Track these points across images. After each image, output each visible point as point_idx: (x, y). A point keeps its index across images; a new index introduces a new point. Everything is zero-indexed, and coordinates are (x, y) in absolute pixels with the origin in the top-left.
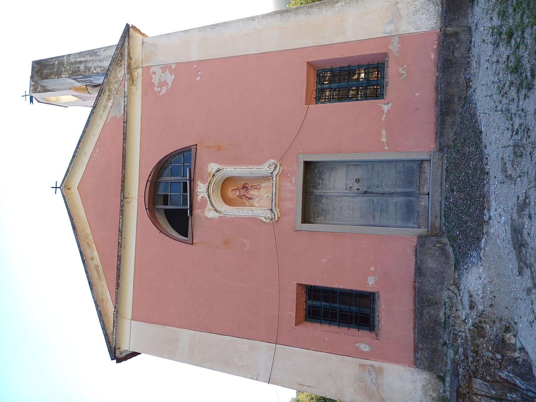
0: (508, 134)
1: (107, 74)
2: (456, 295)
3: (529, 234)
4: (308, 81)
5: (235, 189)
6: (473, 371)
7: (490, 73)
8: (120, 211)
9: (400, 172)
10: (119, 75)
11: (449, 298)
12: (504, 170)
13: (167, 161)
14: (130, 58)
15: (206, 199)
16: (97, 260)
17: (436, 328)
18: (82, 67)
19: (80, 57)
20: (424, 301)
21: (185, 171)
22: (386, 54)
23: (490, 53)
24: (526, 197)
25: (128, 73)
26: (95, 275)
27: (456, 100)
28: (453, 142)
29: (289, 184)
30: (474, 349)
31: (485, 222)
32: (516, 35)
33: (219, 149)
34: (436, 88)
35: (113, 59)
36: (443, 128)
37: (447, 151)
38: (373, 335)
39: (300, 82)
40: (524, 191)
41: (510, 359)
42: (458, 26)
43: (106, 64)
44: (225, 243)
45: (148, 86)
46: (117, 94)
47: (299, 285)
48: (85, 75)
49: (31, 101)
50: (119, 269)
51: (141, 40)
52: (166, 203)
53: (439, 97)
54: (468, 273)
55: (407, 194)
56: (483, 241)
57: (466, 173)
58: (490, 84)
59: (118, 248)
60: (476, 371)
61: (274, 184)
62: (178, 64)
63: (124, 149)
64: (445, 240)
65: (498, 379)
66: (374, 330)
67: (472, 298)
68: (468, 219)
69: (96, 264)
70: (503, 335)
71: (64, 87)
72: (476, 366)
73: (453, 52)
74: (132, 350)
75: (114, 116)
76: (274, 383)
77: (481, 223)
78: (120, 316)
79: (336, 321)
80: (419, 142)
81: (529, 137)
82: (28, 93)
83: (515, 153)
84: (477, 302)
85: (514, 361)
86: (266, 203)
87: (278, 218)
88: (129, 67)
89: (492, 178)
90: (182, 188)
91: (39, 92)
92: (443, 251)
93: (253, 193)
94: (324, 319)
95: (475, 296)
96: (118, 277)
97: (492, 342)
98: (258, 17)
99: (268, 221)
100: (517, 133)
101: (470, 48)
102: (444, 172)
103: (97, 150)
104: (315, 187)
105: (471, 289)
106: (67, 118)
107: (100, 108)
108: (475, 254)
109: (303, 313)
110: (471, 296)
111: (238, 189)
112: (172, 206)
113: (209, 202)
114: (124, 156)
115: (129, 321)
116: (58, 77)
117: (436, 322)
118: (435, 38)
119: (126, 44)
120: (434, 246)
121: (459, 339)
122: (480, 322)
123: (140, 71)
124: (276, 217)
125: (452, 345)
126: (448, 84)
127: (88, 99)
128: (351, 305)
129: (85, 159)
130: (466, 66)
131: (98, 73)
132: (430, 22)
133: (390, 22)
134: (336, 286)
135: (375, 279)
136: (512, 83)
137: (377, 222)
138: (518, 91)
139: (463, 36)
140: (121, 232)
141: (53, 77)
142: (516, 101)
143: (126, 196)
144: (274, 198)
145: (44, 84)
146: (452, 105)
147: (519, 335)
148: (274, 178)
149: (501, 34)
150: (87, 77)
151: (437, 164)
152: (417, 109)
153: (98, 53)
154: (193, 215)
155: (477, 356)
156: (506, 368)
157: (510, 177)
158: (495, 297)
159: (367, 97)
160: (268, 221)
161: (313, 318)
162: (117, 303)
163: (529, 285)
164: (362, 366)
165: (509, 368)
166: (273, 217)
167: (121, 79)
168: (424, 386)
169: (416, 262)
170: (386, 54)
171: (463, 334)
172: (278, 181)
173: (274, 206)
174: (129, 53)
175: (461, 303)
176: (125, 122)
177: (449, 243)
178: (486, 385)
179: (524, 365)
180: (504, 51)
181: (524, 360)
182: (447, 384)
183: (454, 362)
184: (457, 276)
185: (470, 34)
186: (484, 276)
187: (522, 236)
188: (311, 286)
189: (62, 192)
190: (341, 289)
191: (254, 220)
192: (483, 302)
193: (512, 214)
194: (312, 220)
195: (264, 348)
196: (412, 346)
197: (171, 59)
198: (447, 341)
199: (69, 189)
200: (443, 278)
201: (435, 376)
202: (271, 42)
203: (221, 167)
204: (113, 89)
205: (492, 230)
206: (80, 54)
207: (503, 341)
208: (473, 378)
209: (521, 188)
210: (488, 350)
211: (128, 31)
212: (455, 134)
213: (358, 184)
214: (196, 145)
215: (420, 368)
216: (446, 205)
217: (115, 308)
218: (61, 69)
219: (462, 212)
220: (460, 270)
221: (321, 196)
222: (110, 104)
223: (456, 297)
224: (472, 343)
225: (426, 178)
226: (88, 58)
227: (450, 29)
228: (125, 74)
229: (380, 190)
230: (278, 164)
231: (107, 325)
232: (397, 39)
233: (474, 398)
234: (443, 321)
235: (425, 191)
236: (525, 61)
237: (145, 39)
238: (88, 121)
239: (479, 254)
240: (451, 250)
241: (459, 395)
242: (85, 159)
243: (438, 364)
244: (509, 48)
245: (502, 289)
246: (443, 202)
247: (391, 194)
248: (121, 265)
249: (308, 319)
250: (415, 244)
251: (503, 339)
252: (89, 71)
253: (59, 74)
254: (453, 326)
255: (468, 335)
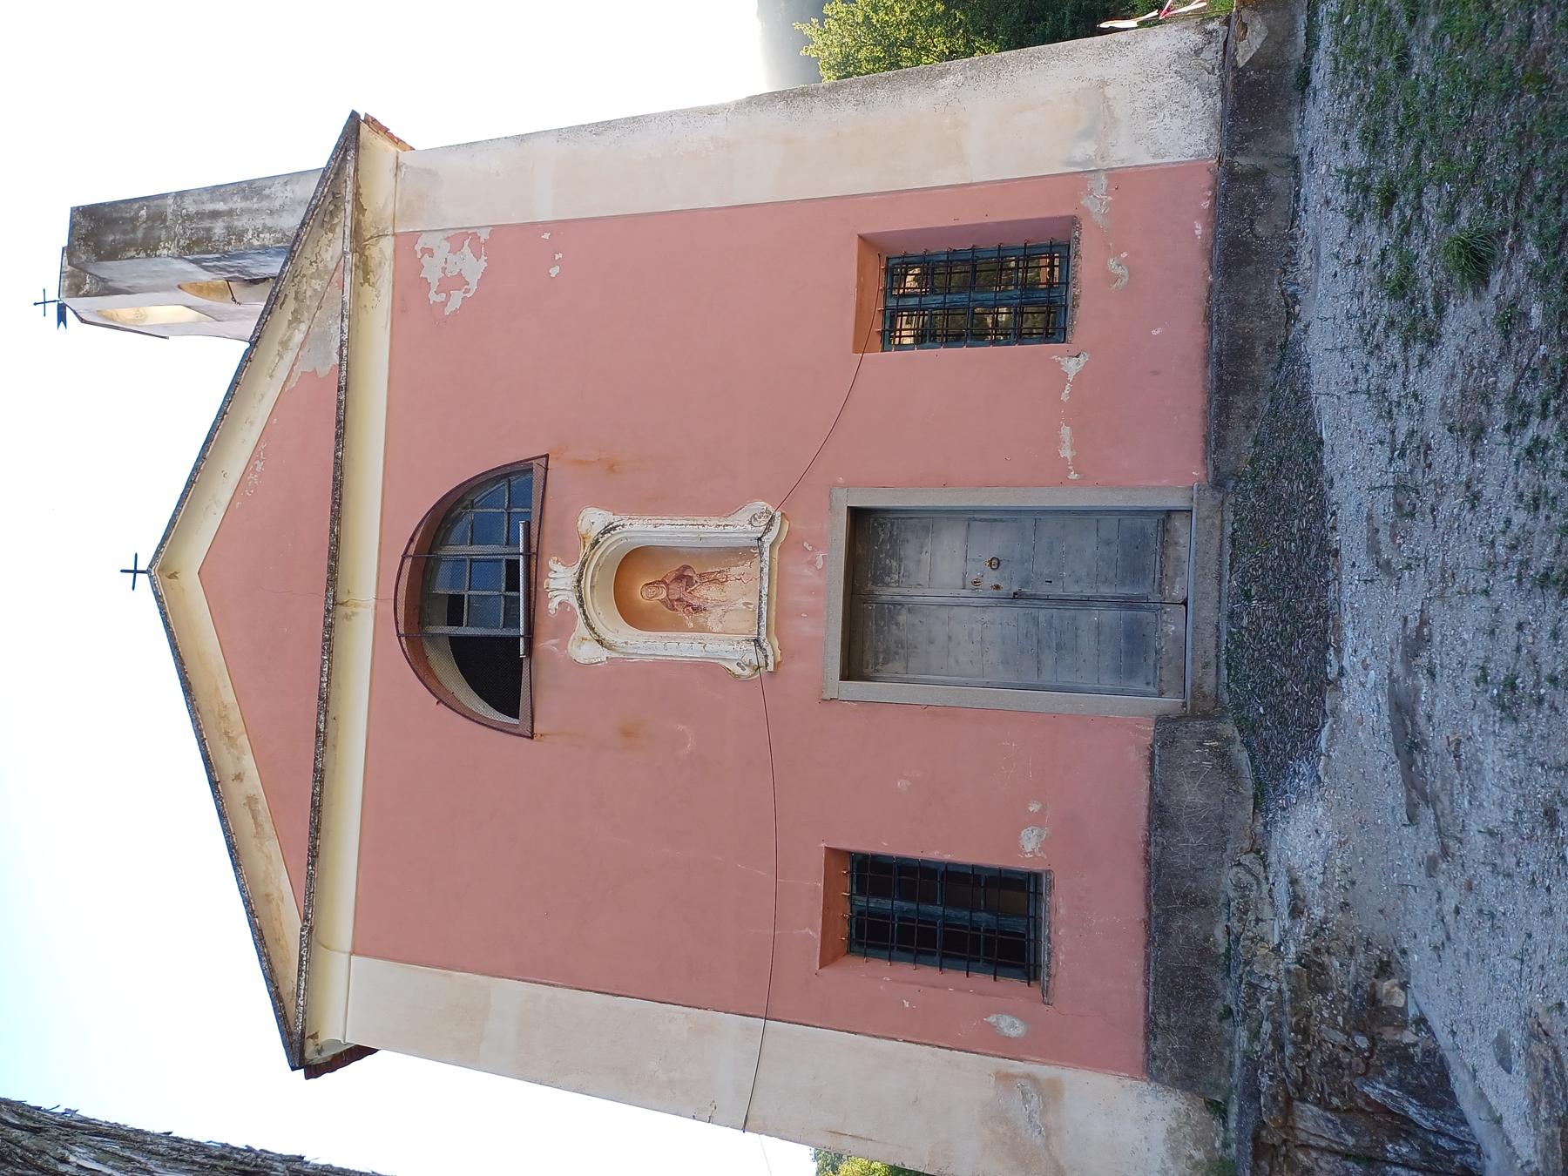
0: (1382, 453)
1: (291, 249)
2: (1257, 879)
3: (1429, 718)
4: (861, 288)
5: (653, 583)
6: (1295, 1083)
7: (1342, 290)
8: (325, 640)
9: (1108, 543)
10: (327, 256)
11: (1240, 887)
12: (1373, 548)
13: (460, 501)
14: (359, 207)
15: (573, 609)
16: (253, 782)
17: (1205, 969)
18: (219, 228)
19: (213, 201)
20: (1171, 895)
21: (511, 529)
22: (1073, 222)
23: (1341, 237)
24: (1424, 623)
25: (354, 251)
26: (246, 823)
27: (1259, 350)
28: (1251, 463)
29: (807, 571)
30: (1297, 1023)
31: (1330, 683)
32: (1402, 199)
33: (611, 469)
34: (1208, 317)
35: (311, 211)
36: (1225, 427)
37: (1234, 488)
38: (1035, 990)
39: (838, 288)
40: (1418, 607)
41: (1392, 1050)
42: (1264, 154)
43: (291, 222)
44: (627, 733)
45: (410, 287)
46: (319, 308)
47: (832, 852)
48: (225, 252)
49: (62, 318)
50: (316, 808)
51: (393, 160)
52: (455, 620)
53: (1215, 342)
54: (1286, 820)
55: (1129, 603)
56: (1325, 732)
57: (1282, 550)
58: (1341, 317)
59: (317, 748)
60: (1304, 1083)
61: (766, 570)
62: (496, 229)
63: (339, 464)
64: (1229, 729)
65: (1361, 1103)
66: (1036, 978)
67: (1298, 888)
68: (1287, 672)
69: (251, 792)
70: (1373, 986)
71: (159, 282)
72: (1303, 1068)
73: (1252, 224)
74: (354, 1040)
75: (309, 370)
76: (760, 1131)
77: (1320, 684)
78: (319, 942)
79: (933, 954)
80: (1159, 461)
81: (1430, 466)
82: (53, 294)
83: (1398, 506)
84: (1309, 896)
85: (1401, 1055)
86: (743, 622)
87: (777, 665)
88: (356, 232)
89: (1347, 567)
90: (504, 573)
91: (86, 295)
92: (1222, 755)
93: (706, 593)
94: (899, 949)
95: (1304, 882)
96: (316, 829)
97: (1346, 1005)
98: (725, 107)
99: (748, 672)
100: (1402, 455)
101: (1295, 212)
102: (1227, 545)
103: (260, 465)
104: (878, 580)
105: (1295, 862)
106: (173, 371)
107: (271, 346)
108: (1304, 768)
109: (842, 931)
110: (1294, 882)
111: (663, 581)
112: (472, 621)
113: (581, 619)
114: (338, 485)
115: (345, 957)
116: (148, 256)
117: (1204, 952)
118: (1205, 180)
119: (350, 169)
120: (1201, 745)
121: (1263, 1000)
122: (1317, 951)
123: (387, 245)
124: (771, 661)
125: (1246, 1015)
126: (1238, 307)
127: (231, 317)
128: (974, 908)
129: (222, 491)
130: (1285, 260)
131: (264, 247)
132: (1191, 139)
133: (1086, 134)
134: (935, 854)
135: (1040, 836)
136: (1392, 323)
137: (1048, 677)
138: (1406, 345)
139: (1278, 181)
140: (324, 700)
141: (133, 253)
142: (1400, 371)
143: (341, 598)
144: (764, 607)
145: (104, 274)
146: (1248, 363)
147: (1412, 983)
148: (767, 554)
149: (1366, 190)
150: (232, 257)
151: (1209, 522)
152: (1157, 373)
153: (267, 192)
154: (534, 656)
155: (1306, 1040)
156: (1383, 1074)
157: (1386, 567)
158: (1353, 883)
159: (1021, 335)
160: (748, 672)
161: (869, 946)
162: (310, 905)
163: (1431, 851)
164: (1004, 1078)
165: (1389, 1074)
166: (762, 663)
167: (332, 266)
168: (1171, 1131)
169: (1151, 789)
170: (1073, 222)
171: (1274, 986)
172: (775, 562)
173: (763, 630)
174: (357, 195)
175: (1268, 900)
176: (343, 388)
177: (1239, 738)
178: (1329, 1120)
179: (1428, 1065)
180: (1375, 237)
181: (1428, 1053)
182: (1232, 1124)
183: (1249, 1058)
184: (1259, 829)
185: (1295, 177)
186: (1328, 826)
187: (1414, 723)
188: (865, 856)
189: (153, 585)
190: (948, 865)
191: (709, 670)
192: (1325, 898)
193: (1392, 663)
194: (869, 671)
195: (732, 1032)
196: (1141, 1020)
197: (480, 214)
198: (1233, 1007)
199: (173, 576)
200: (1224, 832)
201: (1201, 1102)
202: (760, 179)
203: (615, 519)
204: (309, 293)
205: (1346, 706)
206: (215, 191)
207: (1373, 1000)
208: (1296, 1103)
209: (1410, 597)
210: (1335, 1026)
211: (355, 133)
212: (1256, 443)
213: (997, 573)
214: (547, 456)
215: (1163, 1083)
216: (1230, 634)
217: (306, 919)
218: (157, 233)
219: (1271, 656)
220: (1268, 810)
221: (895, 604)
222: (298, 337)
223: (1259, 884)
224: (1293, 1008)
225: (1178, 559)
226: (237, 204)
227: (1243, 162)
228: (344, 253)
229: (1056, 591)
230: (778, 514)
231: (278, 968)
232: (1104, 180)
233: (1301, 1156)
234: (1222, 950)
235: (1177, 593)
236: (1421, 271)
237: (405, 157)
238: (235, 383)
239: (1314, 767)
240: (1244, 756)
241: (1260, 1150)
242: (222, 491)
243: (1208, 1069)
244: (1385, 230)
245: (1370, 863)
246: (1224, 626)
247: (1085, 602)
248: (324, 795)
249: (856, 948)
250: (1149, 740)
251: (1374, 995)
252: (241, 241)
253: (149, 248)
254: (1247, 963)
255: (1284, 986)
